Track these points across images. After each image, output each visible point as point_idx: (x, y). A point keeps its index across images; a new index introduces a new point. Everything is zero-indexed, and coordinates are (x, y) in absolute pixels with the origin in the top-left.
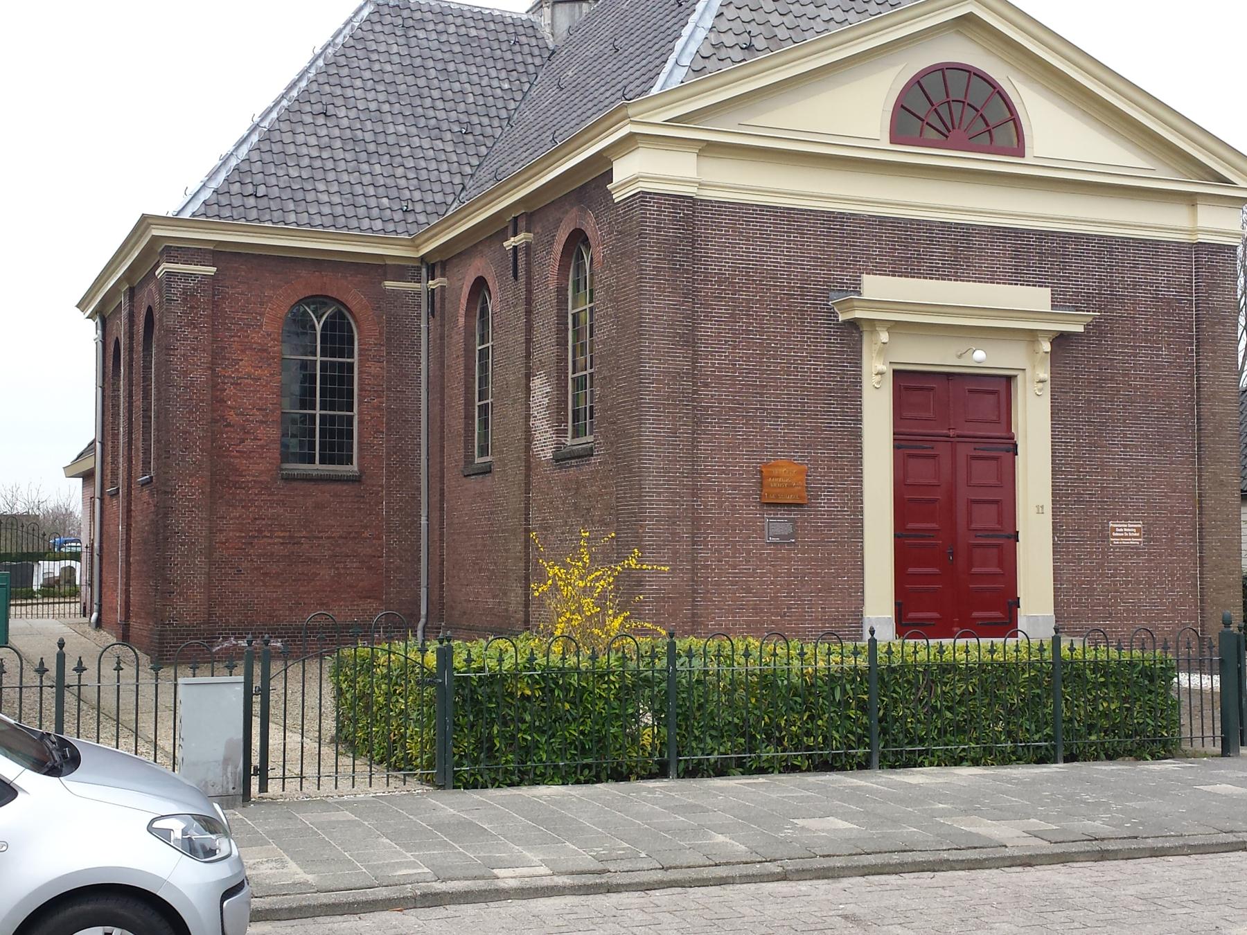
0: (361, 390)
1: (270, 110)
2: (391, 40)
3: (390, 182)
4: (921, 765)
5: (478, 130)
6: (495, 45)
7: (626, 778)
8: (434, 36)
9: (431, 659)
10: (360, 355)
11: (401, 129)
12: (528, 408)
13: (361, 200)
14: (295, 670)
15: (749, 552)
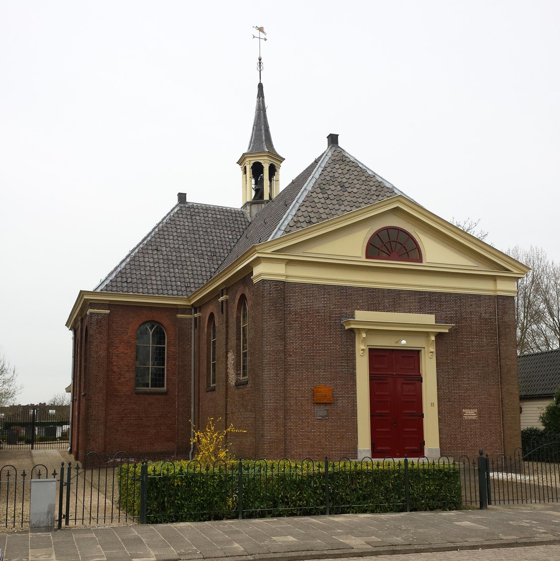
0: (168, 357)
1: (135, 249)
2: (185, 220)
3: (181, 275)
4: (349, 513)
5: (218, 254)
6: (227, 221)
7: (221, 519)
8: (203, 218)
9: (139, 470)
10: (167, 344)
11: (187, 255)
12: (227, 365)
13: (169, 283)
14: (95, 472)
15: (308, 423)
